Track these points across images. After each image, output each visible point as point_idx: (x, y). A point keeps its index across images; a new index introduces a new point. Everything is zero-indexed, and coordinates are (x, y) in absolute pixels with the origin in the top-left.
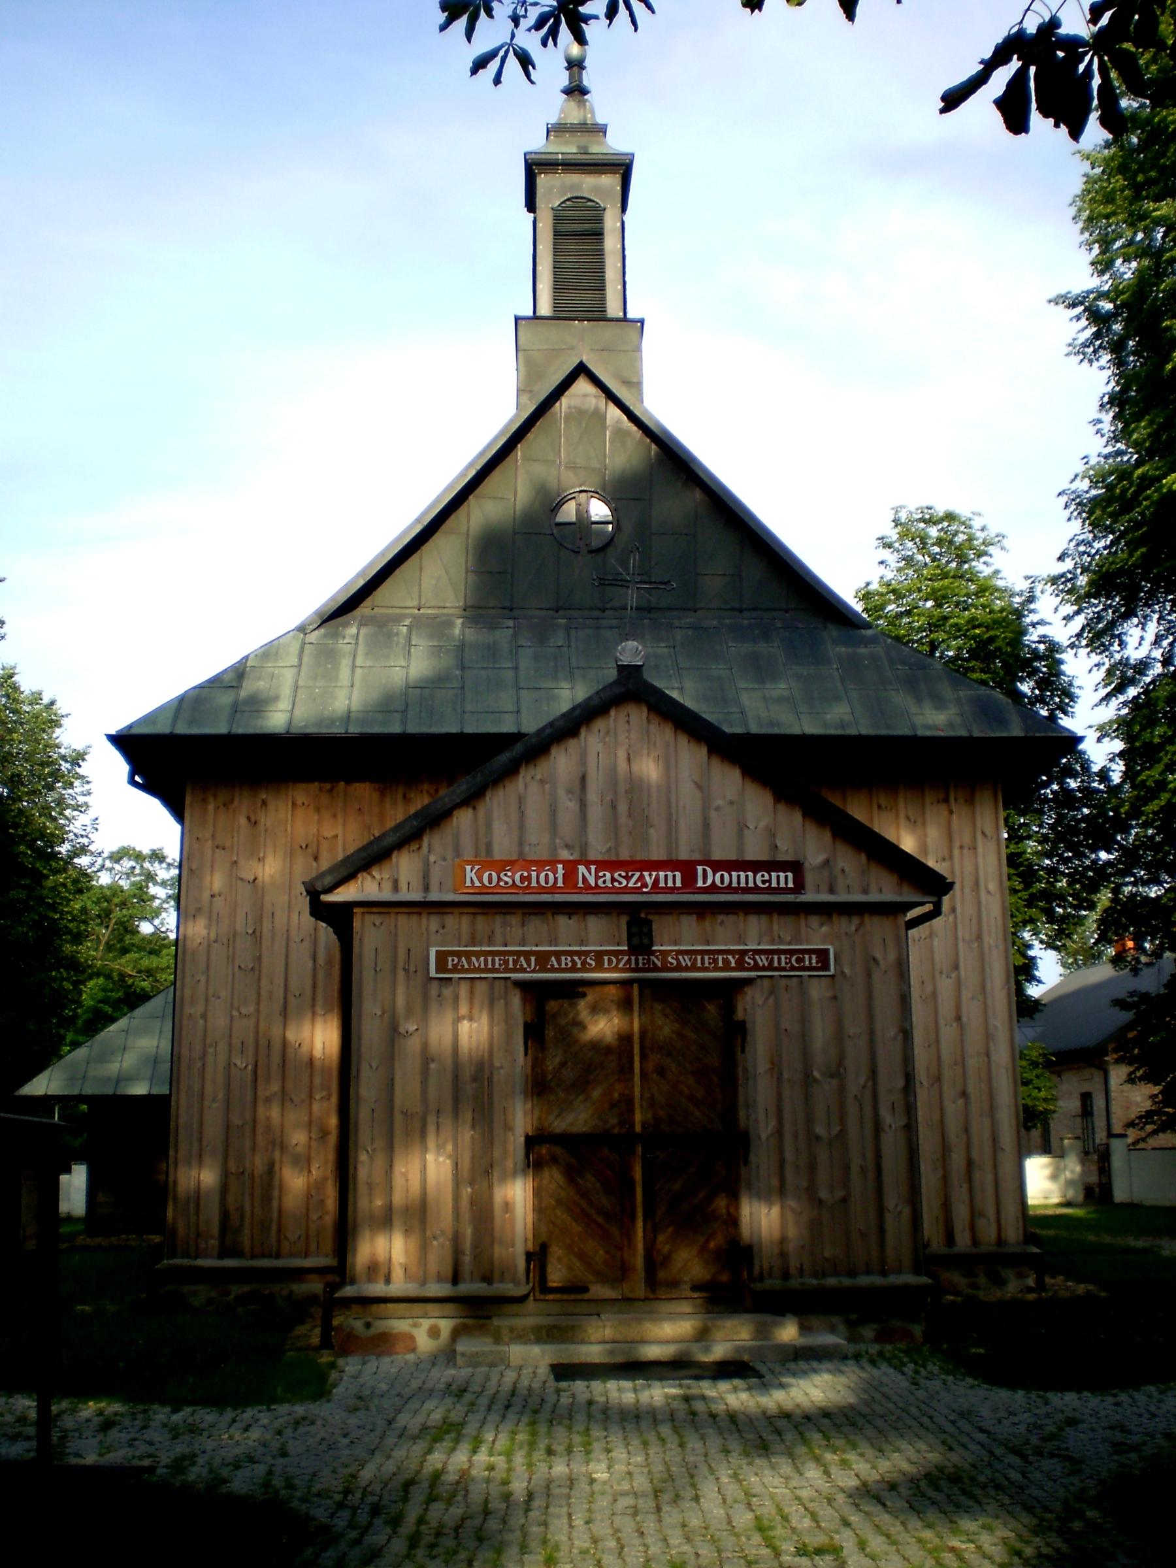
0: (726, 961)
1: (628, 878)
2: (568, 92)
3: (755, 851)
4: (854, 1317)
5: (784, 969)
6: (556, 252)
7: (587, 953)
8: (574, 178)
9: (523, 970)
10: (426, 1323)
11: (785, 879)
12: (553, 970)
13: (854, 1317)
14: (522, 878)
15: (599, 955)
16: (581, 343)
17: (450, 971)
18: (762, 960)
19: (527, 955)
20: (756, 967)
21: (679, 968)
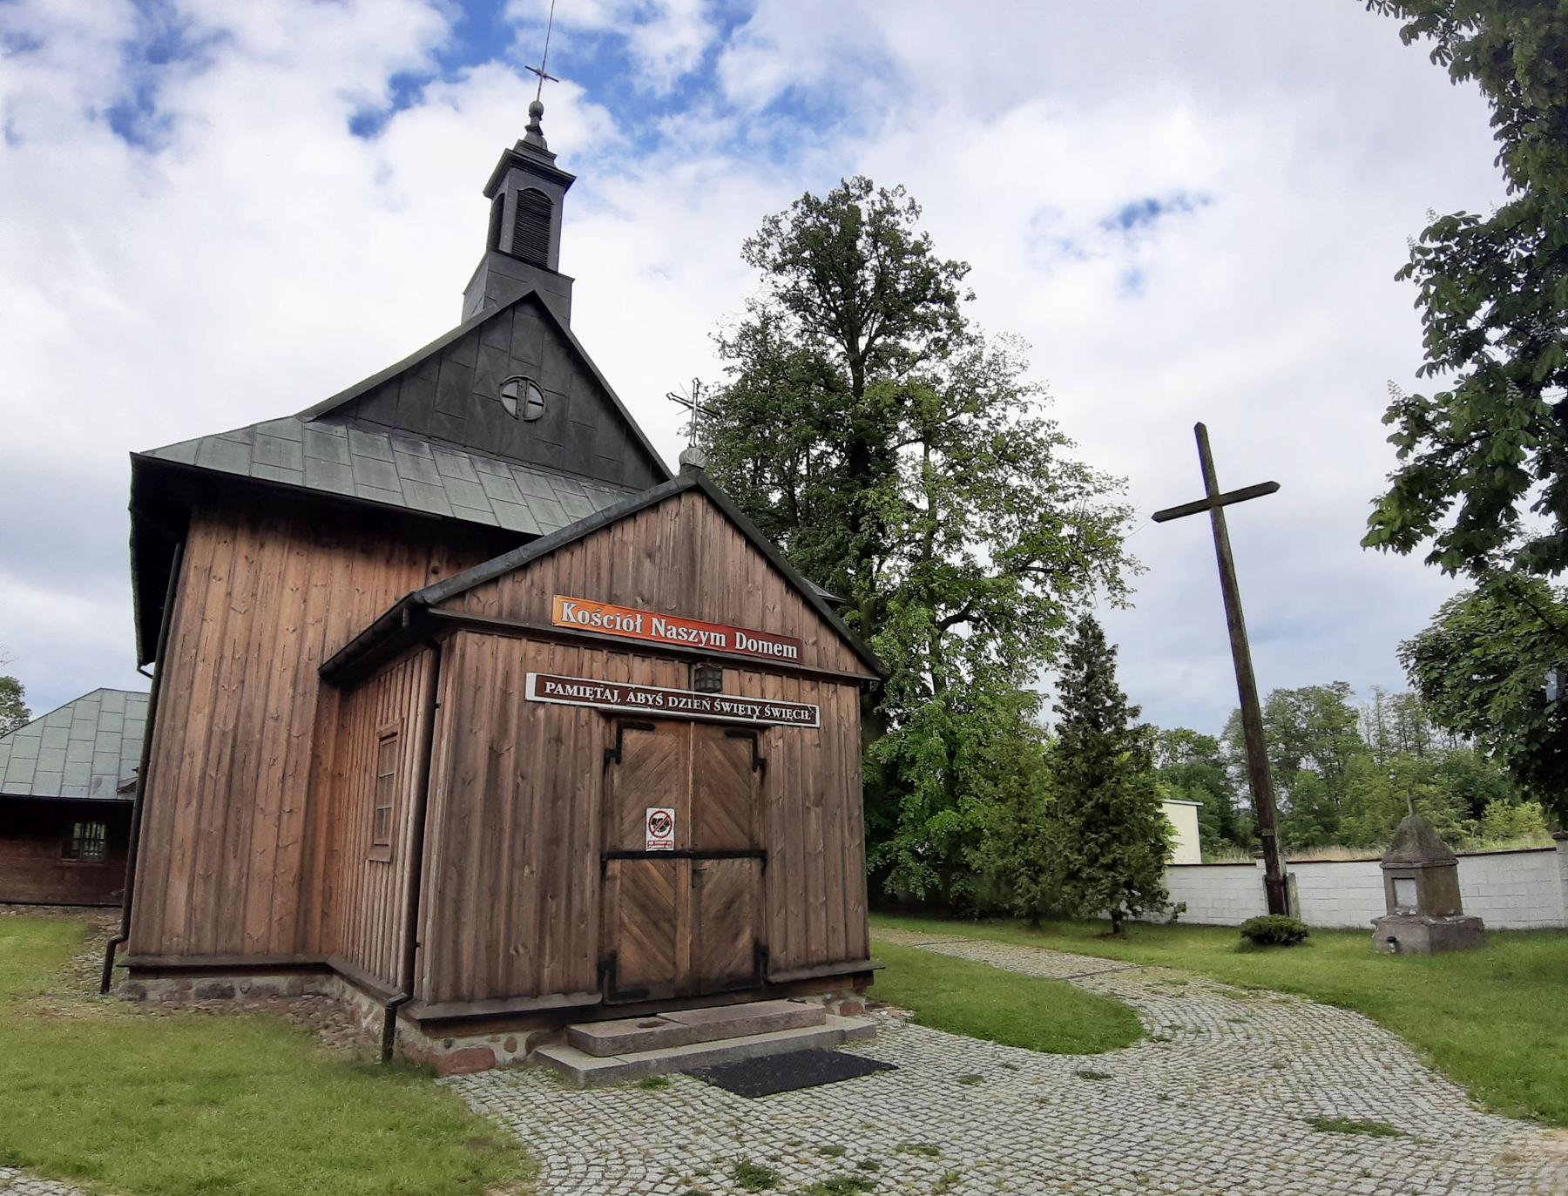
0: (753, 711)
1: (689, 634)
2: (528, 128)
3: (773, 626)
4: (829, 996)
5: (587, 700)
6: (518, 216)
7: (704, 698)
8: (536, 179)
9: (608, 702)
10: (504, 1037)
11: (790, 651)
12: (631, 703)
13: (829, 996)
14: (610, 622)
15: (666, 695)
16: (531, 281)
17: (547, 695)
18: (776, 712)
19: (611, 688)
20: (772, 717)
21: (721, 712)
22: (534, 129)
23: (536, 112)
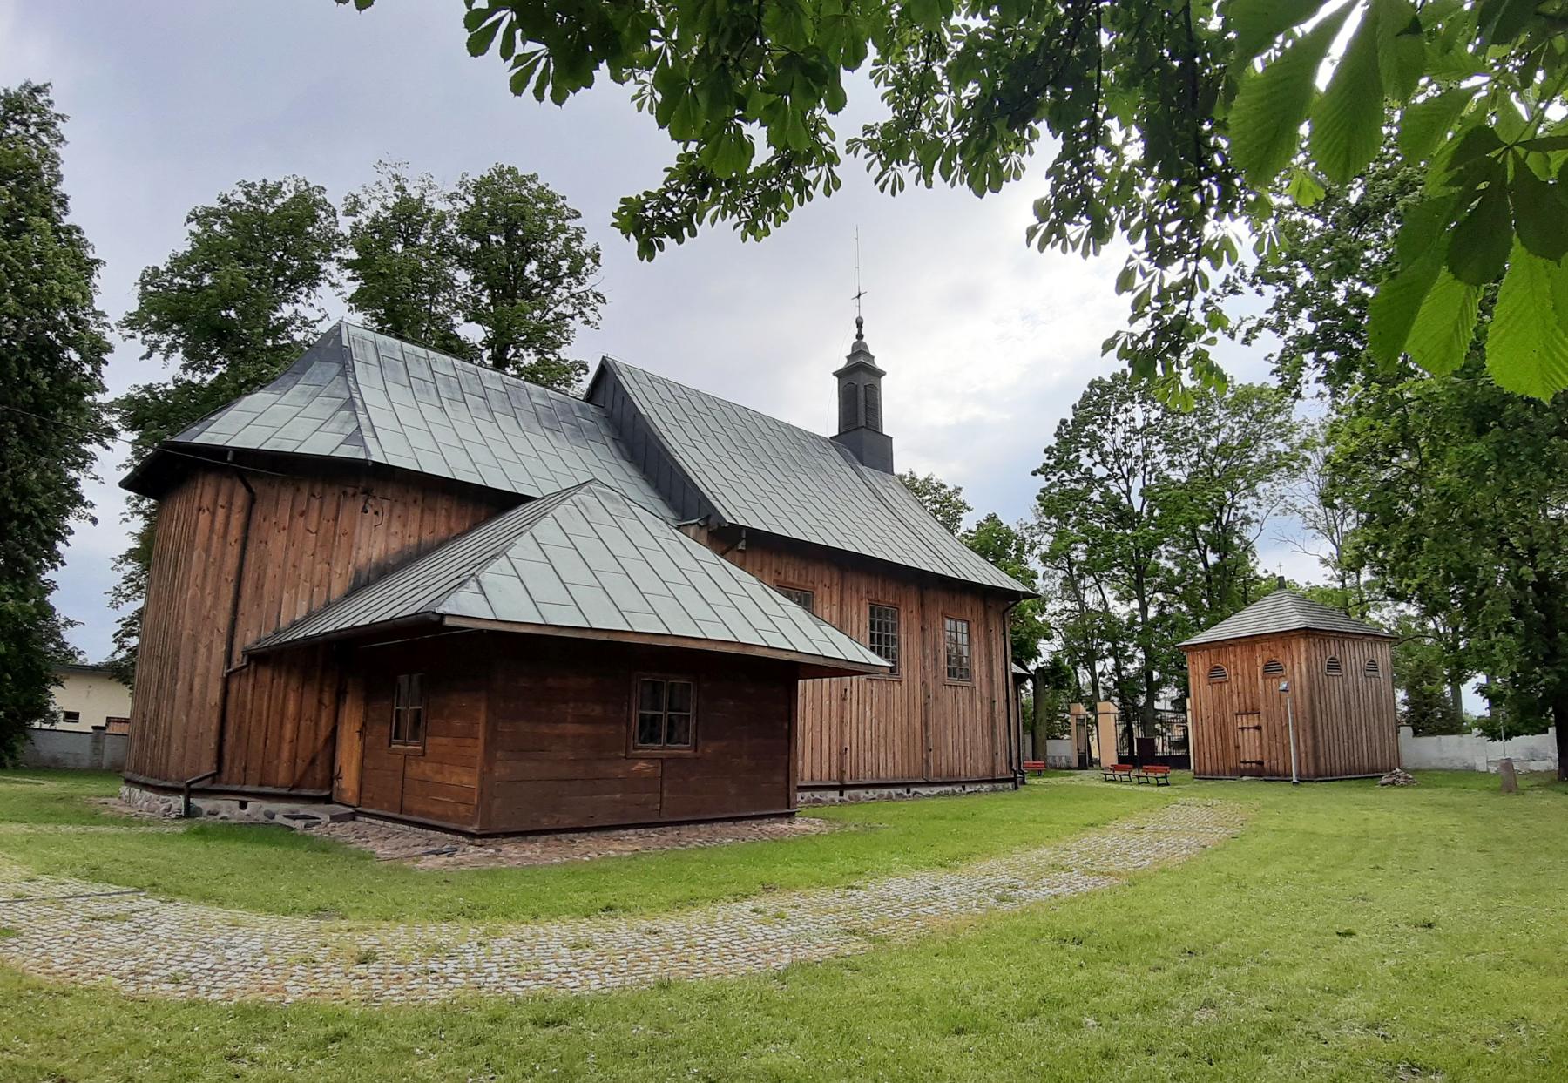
22: (860, 336)
23: (860, 324)
